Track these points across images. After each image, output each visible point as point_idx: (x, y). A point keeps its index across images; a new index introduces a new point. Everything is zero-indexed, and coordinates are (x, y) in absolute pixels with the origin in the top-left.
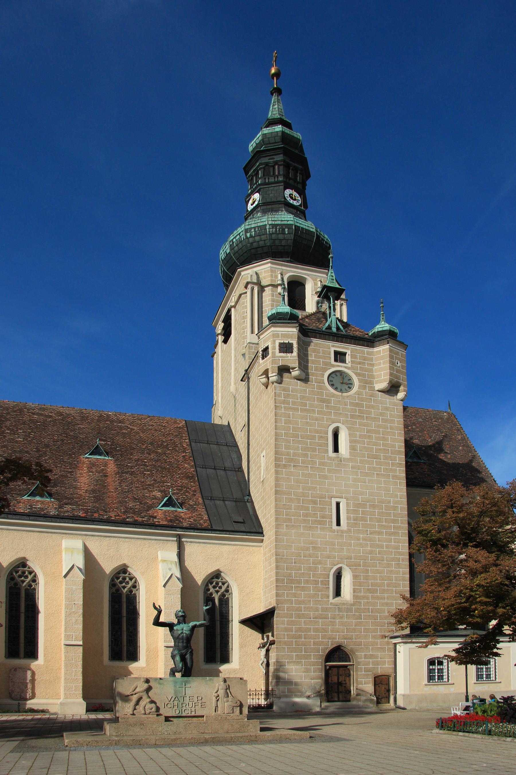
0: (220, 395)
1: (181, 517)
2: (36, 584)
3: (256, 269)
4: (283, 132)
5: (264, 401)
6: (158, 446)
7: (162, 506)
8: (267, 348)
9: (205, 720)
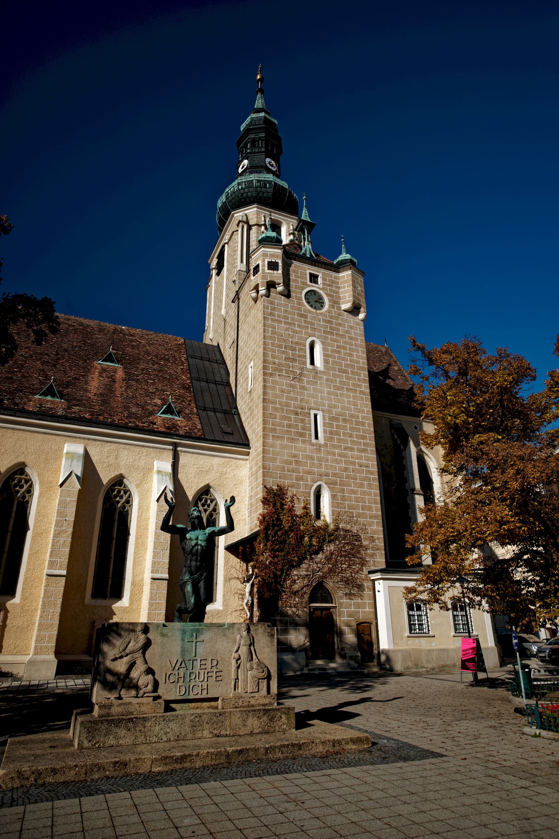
0: (212, 320)
1: (178, 425)
2: (30, 496)
3: (246, 212)
4: (265, 117)
5: (254, 314)
6: (161, 359)
7: (161, 414)
8: (258, 266)
9: (220, 707)
